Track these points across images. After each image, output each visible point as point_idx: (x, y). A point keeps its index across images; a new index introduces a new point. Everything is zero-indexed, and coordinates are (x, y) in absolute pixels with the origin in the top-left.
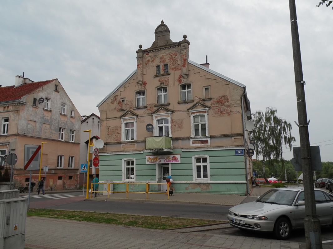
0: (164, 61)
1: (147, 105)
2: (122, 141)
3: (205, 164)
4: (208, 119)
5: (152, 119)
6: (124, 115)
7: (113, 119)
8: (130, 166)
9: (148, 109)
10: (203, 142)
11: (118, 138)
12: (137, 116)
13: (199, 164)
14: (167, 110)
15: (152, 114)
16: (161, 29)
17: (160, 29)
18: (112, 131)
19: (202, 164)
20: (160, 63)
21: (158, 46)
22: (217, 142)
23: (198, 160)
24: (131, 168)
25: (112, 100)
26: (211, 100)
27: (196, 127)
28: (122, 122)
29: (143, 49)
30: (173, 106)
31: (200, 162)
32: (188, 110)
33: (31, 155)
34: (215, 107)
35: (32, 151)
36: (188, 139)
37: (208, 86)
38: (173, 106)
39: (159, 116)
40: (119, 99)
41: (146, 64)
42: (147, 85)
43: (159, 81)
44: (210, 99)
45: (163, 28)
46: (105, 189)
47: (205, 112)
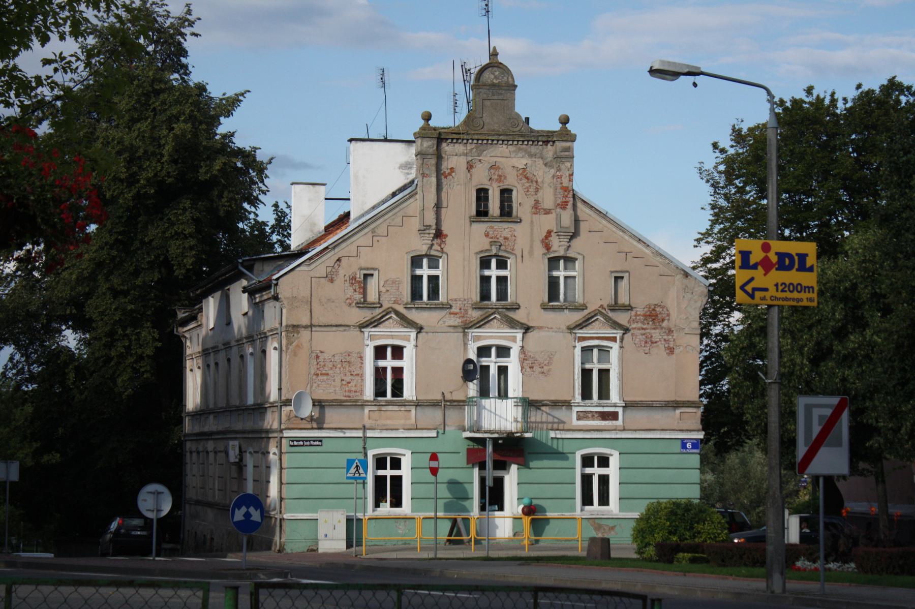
0: (500, 178)
3: (603, 471)
4: (622, 359)
6: (375, 323)
7: (334, 329)
9: (450, 313)
10: (604, 416)
11: (353, 389)
14: (513, 324)
15: (466, 327)
16: (492, 76)
17: (488, 76)
20: (489, 183)
21: (485, 130)
22: (640, 417)
24: (391, 477)
25: (329, 269)
27: (586, 374)
29: (432, 123)
30: (528, 314)
32: (571, 329)
33: (816, 429)
34: (639, 329)
35: (821, 417)
36: (568, 404)
37: (622, 272)
38: (528, 314)
40: (355, 268)
42: (448, 240)
43: (487, 235)
44: (628, 308)
45: (497, 73)
46: (326, 536)
47: (614, 339)
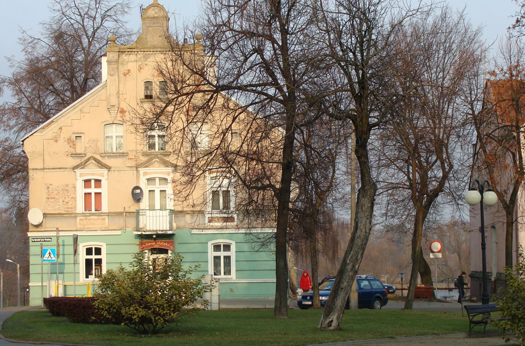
1: (128, 152)
2: (77, 212)
3: (227, 254)
5: (138, 177)
8: (94, 257)
11: (70, 206)
12: (109, 168)
13: (217, 254)
18: (56, 192)
19: (222, 254)
20: (152, 78)
23: (217, 248)
25: (54, 134)
26: (72, 154)
28: (78, 178)
31: (220, 250)
39: (151, 173)
41: (125, 75)
